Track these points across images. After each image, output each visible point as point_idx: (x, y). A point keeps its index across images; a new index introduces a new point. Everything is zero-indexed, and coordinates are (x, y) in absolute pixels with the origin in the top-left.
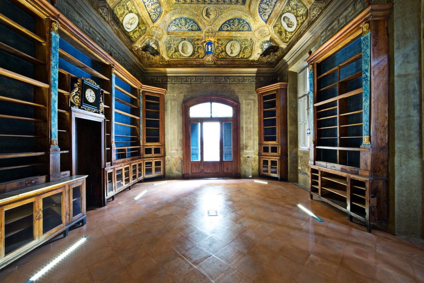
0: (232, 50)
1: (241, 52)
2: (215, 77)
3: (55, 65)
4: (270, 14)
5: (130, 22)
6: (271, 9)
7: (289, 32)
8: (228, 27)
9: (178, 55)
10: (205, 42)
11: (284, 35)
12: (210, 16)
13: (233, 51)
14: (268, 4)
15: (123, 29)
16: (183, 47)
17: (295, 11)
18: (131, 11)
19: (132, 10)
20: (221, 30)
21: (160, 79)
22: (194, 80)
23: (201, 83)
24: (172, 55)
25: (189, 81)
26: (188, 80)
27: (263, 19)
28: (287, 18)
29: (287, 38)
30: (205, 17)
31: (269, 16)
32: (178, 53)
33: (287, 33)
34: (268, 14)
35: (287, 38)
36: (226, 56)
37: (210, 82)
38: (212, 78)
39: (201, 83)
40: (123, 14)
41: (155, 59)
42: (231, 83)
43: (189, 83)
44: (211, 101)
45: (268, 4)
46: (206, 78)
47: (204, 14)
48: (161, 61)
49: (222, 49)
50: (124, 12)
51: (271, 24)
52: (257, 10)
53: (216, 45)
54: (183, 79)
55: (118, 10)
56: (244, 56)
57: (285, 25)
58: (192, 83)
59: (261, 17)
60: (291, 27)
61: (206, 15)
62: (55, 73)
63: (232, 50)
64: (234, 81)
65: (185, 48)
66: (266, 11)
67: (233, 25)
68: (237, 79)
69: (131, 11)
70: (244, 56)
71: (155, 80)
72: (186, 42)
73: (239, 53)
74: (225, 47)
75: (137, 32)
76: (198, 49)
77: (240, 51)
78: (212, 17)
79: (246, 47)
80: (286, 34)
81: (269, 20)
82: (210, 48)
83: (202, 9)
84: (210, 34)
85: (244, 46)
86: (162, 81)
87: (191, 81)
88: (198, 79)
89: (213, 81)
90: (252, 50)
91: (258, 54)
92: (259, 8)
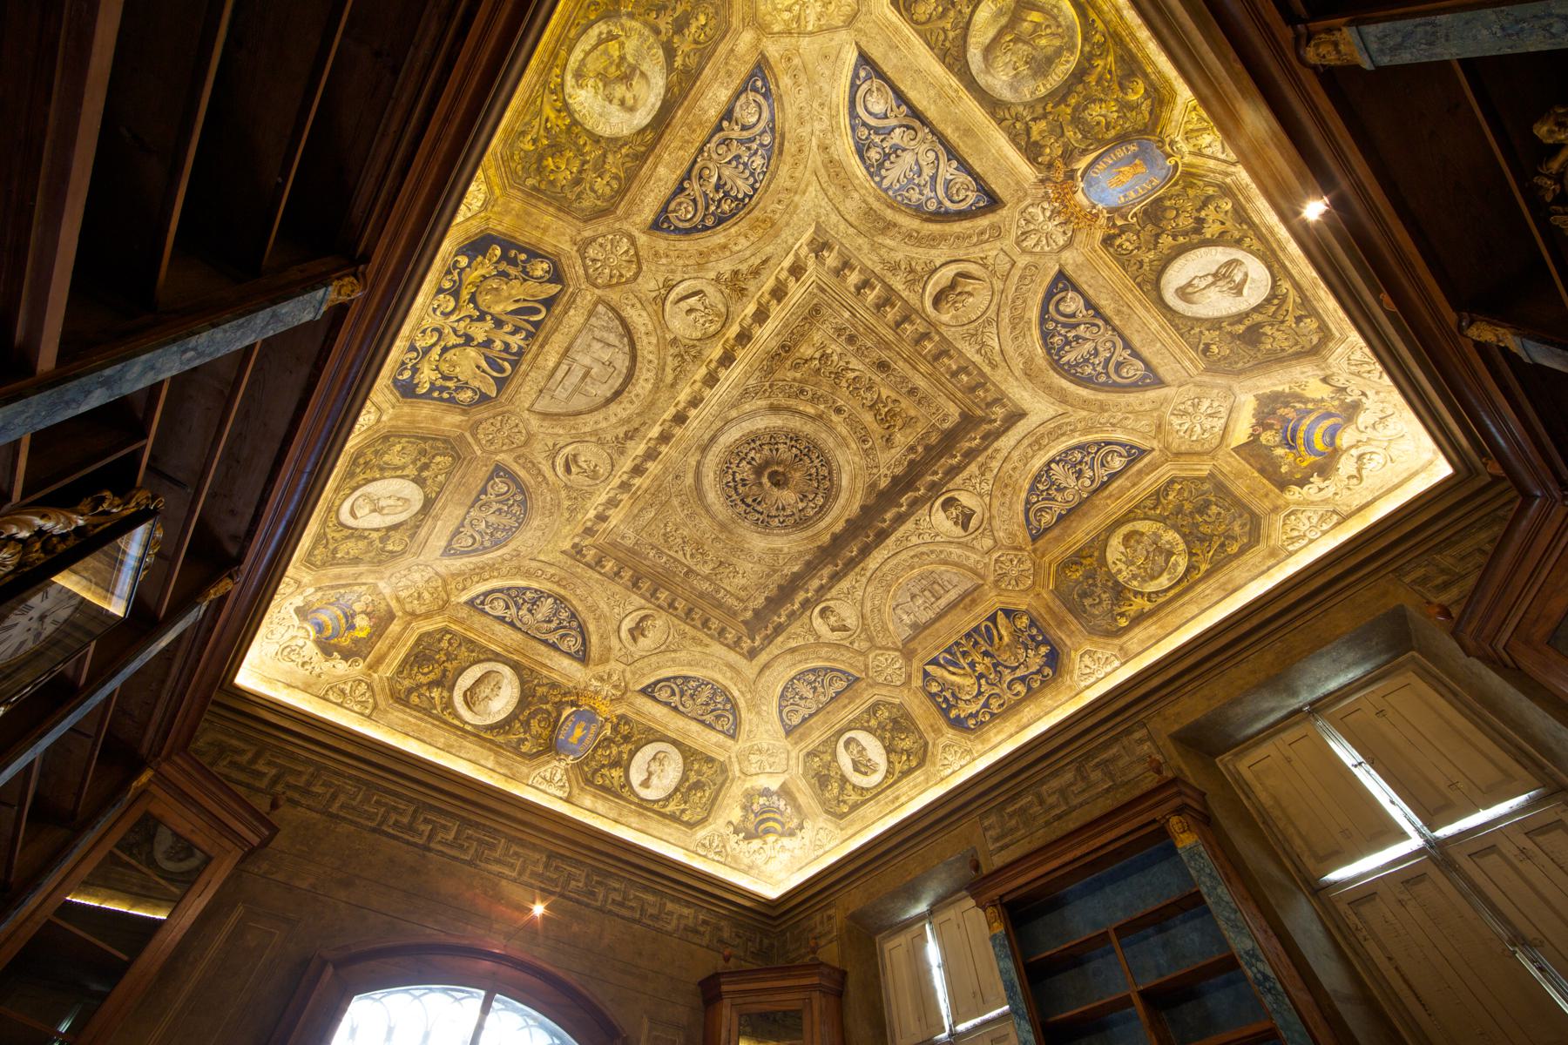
0: (650, 774)
1: (679, 795)
2: (549, 857)
3: (200, 349)
4: (811, 716)
5: (382, 503)
6: (818, 702)
7: (854, 786)
8: (673, 693)
9: (437, 701)
10: (573, 704)
11: (836, 791)
12: (641, 639)
13: (654, 780)
14: (815, 688)
15: (337, 502)
16: (479, 682)
17: (888, 735)
18: (425, 479)
19: (429, 482)
20: (648, 692)
21: (270, 763)
22: (451, 837)
23: (476, 866)
24: (410, 691)
25: (421, 834)
26: (422, 827)
27: (782, 720)
28: (858, 744)
29: (844, 802)
30: (624, 634)
31: (804, 720)
32: (445, 694)
33: (849, 787)
34: (805, 712)
35: (844, 802)
36: (623, 787)
37: (520, 874)
38: (537, 856)
39: (476, 866)
40: (396, 468)
41: (318, 670)
42: (610, 911)
43: (416, 840)
44: (493, 987)
45: (815, 688)
46: (508, 849)
47: (627, 624)
48: (342, 691)
49: (620, 753)
50: (403, 468)
51: (803, 744)
52: (779, 689)
53: (608, 732)
54: (395, 809)
55: (398, 447)
56: (683, 811)
57: (845, 761)
58: (430, 850)
59: (781, 712)
60: (865, 774)
61: (631, 631)
62: (152, 368)
63: (650, 774)
64: (621, 905)
65: (485, 690)
66: (802, 703)
67: (692, 696)
68: (636, 897)
69: (425, 479)
70: (683, 811)
71: (237, 758)
72: (507, 671)
73: (670, 796)
74: (632, 754)
75: (362, 544)
76: (533, 715)
77: (677, 789)
78: (645, 643)
79: (699, 781)
80: (842, 788)
81: (801, 730)
82: (578, 733)
83: (631, 608)
84: (607, 687)
85: (693, 778)
86: (275, 781)
87: (430, 838)
88: (469, 838)
89: (533, 874)
90: (713, 804)
91: (730, 823)
92: (785, 689)
